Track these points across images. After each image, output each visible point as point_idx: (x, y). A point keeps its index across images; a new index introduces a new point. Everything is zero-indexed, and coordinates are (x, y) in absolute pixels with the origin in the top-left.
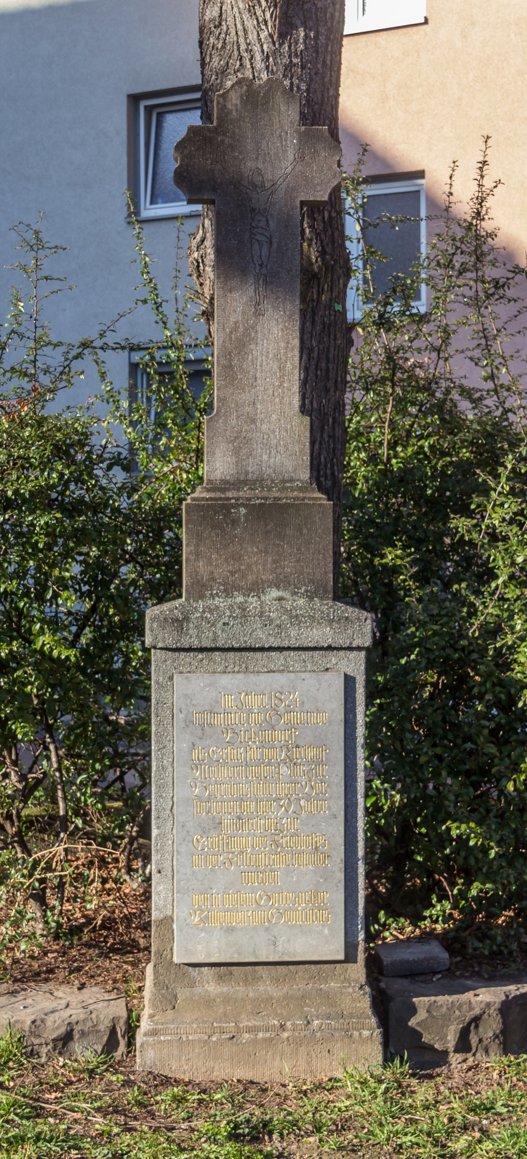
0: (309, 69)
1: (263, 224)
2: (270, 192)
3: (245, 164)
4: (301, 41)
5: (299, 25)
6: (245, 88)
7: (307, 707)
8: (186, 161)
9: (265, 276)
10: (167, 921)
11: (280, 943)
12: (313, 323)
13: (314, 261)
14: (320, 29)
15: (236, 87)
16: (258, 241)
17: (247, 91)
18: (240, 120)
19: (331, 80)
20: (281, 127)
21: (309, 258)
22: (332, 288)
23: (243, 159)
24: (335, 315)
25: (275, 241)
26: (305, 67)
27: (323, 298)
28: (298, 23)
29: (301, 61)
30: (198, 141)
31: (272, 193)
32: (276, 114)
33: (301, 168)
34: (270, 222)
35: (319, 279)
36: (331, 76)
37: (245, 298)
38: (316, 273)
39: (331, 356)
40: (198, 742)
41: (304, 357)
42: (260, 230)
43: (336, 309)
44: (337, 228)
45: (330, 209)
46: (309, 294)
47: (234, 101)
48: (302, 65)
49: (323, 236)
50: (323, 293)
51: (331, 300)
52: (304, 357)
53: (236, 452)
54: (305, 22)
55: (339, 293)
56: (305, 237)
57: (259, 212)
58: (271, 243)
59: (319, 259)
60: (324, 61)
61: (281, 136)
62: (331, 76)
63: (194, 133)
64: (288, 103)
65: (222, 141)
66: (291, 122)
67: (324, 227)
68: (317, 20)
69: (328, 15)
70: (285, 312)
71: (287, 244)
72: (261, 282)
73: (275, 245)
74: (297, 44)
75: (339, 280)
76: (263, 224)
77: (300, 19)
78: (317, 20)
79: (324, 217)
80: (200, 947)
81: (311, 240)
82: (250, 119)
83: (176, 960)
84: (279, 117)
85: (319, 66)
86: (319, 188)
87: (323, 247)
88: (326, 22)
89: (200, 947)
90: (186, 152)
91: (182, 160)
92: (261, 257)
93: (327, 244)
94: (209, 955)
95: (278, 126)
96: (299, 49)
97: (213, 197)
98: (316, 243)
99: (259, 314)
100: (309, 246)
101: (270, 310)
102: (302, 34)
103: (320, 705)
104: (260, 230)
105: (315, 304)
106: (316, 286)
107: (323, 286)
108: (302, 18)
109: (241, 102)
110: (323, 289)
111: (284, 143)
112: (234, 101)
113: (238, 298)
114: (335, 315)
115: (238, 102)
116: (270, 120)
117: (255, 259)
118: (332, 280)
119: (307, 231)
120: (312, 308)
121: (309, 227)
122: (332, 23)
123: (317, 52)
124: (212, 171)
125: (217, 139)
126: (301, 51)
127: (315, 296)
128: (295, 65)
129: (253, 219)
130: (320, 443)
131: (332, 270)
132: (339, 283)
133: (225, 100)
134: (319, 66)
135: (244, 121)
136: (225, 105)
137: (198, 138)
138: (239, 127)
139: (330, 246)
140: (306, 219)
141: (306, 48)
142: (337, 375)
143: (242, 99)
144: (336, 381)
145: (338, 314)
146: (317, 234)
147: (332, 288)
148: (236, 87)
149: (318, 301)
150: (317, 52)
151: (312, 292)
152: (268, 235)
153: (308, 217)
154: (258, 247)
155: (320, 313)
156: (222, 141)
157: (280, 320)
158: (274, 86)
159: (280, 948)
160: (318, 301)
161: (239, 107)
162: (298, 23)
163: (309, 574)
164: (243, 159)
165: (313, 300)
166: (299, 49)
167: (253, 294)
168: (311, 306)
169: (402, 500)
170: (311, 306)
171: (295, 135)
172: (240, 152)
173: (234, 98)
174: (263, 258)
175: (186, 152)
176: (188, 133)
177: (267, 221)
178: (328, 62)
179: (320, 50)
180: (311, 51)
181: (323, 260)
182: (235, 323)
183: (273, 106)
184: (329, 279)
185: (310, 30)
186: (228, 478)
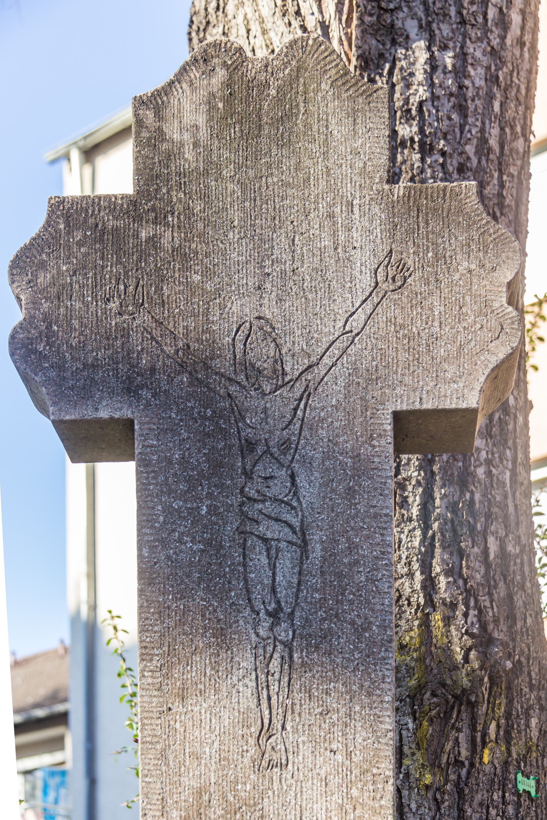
0: (443, 154)
2: (299, 388)
3: (223, 307)
4: (420, 76)
5: (413, 35)
6: (221, 74)
8: (46, 306)
9: (288, 646)
13: (459, 658)
14: (470, 48)
15: (194, 73)
16: (265, 540)
17: (229, 84)
18: (206, 173)
19: (500, 195)
20: (332, 189)
21: (447, 649)
22: (508, 733)
23: (218, 292)
24: (518, 805)
26: (432, 148)
27: (486, 759)
28: (412, 27)
29: (421, 131)
30: (80, 244)
31: (307, 394)
32: (315, 147)
33: (394, 312)
34: (301, 481)
35: (473, 706)
36: (502, 185)
37: (225, 715)
38: (464, 690)
42: (268, 507)
43: (521, 787)
44: (523, 588)
45: (501, 533)
46: (448, 746)
47: (188, 119)
48: (422, 144)
49: (484, 600)
50: (484, 744)
51: (506, 764)
54: (429, 24)
55: (529, 750)
56: (436, 599)
57: (267, 451)
59: (473, 654)
60: (483, 140)
61: (331, 216)
62: (502, 185)
63: (67, 218)
64: (353, 114)
65: (153, 240)
66: (363, 172)
67: (486, 575)
68: (463, 22)
69: (492, 13)
70: (349, 755)
71: (352, 548)
72: (274, 666)
74: (408, 86)
75: (528, 717)
77: (414, 16)
78: (463, 22)
79: (486, 552)
81: (453, 606)
82: (239, 167)
84: (326, 158)
85: (470, 149)
86: (451, 370)
87: (483, 627)
88: (486, 31)
90: (43, 279)
91: (35, 303)
92: (274, 591)
93: (496, 621)
95: (322, 183)
96: (414, 101)
97: (127, 413)
98: (466, 615)
99: (271, 765)
100: (448, 621)
101: (305, 750)
102: (422, 56)
104: (268, 507)
105: (464, 772)
106: (464, 725)
107: (486, 727)
108: (421, 13)
109: (210, 119)
110: (485, 734)
111: (342, 238)
112: (188, 119)
113: (206, 717)
114: (518, 805)
115: (202, 120)
116: (298, 167)
117: (256, 596)
118: (508, 715)
119: (442, 582)
120: (457, 784)
121: (448, 573)
122: (503, 38)
123: (462, 109)
124: (125, 333)
125: (137, 236)
126: (421, 104)
127: (464, 753)
128: (403, 144)
129: (248, 475)
131: (509, 688)
132: (528, 726)
133: (159, 116)
134: (470, 149)
135: (219, 177)
136: (160, 130)
137: (78, 235)
138: (205, 197)
139: (503, 627)
140: (438, 551)
141: (434, 98)
143: (211, 107)
145: (525, 802)
146: (469, 592)
147: (508, 733)
148: (194, 73)
149: (472, 765)
150: (462, 109)
151: (456, 740)
152: (296, 522)
153: (444, 548)
154: (264, 560)
155: (478, 797)
156: (153, 240)
157: (334, 781)
158: (311, 63)
160: (472, 765)
161: (203, 134)
162: (412, 27)
164: (218, 292)
165: (458, 763)
166: (414, 101)
167: (253, 704)
168: (453, 777)
170: (453, 777)
171: (376, 210)
172: (208, 274)
173: (187, 106)
174: (282, 594)
175: (43, 279)
176: (48, 223)
177: (293, 477)
178: (493, 142)
179: (471, 106)
180: (447, 106)
181: (484, 657)
183: (307, 126)
184: (501, 711)
185: (444, 48)
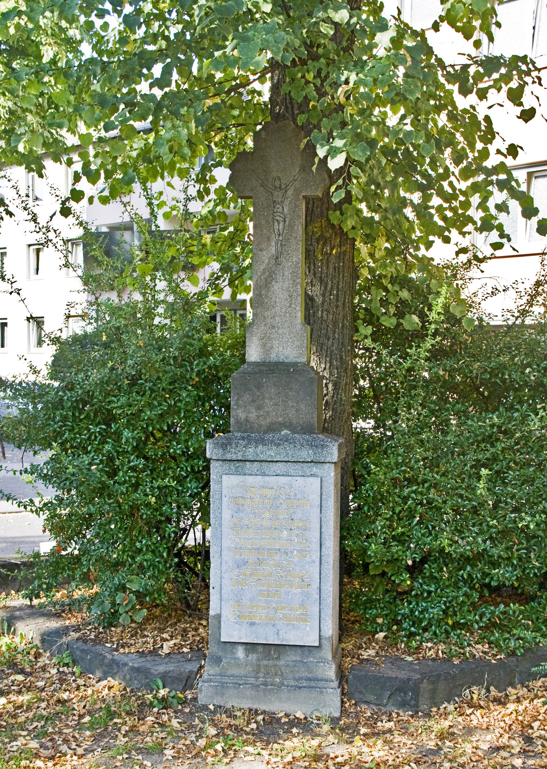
1: (280, 210)
7: (298, 496)
10: (218, 617)
11: (281, 633)
12: (328, 268)
16: (277, 220)
25: (287, 220)
39: (340, 286)
40: (235, 514)
41: (322, 288)
42: (278, 214)
52: (322, 288)
53: (264, 346)
58: (285, 221)
73: (287, 223)
76: (280, 210)
80: (235, 633)
83: (223, 640)
89: (235, 633)
94: (240, 638)
103: (306, 495)
104: (278, 214)
129: (274, 207)
130: (333, 339)
142: (345, 298)
144: (344, 302)
159: (281, 637)
163: (303, 418)
169: (146, 409)
182: (264, 270)
186: (259, 361)
